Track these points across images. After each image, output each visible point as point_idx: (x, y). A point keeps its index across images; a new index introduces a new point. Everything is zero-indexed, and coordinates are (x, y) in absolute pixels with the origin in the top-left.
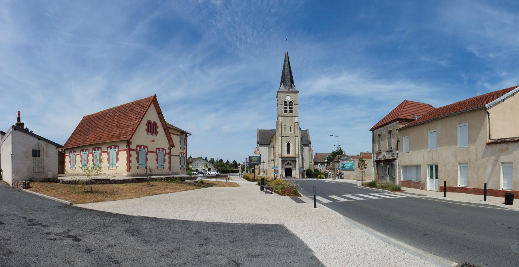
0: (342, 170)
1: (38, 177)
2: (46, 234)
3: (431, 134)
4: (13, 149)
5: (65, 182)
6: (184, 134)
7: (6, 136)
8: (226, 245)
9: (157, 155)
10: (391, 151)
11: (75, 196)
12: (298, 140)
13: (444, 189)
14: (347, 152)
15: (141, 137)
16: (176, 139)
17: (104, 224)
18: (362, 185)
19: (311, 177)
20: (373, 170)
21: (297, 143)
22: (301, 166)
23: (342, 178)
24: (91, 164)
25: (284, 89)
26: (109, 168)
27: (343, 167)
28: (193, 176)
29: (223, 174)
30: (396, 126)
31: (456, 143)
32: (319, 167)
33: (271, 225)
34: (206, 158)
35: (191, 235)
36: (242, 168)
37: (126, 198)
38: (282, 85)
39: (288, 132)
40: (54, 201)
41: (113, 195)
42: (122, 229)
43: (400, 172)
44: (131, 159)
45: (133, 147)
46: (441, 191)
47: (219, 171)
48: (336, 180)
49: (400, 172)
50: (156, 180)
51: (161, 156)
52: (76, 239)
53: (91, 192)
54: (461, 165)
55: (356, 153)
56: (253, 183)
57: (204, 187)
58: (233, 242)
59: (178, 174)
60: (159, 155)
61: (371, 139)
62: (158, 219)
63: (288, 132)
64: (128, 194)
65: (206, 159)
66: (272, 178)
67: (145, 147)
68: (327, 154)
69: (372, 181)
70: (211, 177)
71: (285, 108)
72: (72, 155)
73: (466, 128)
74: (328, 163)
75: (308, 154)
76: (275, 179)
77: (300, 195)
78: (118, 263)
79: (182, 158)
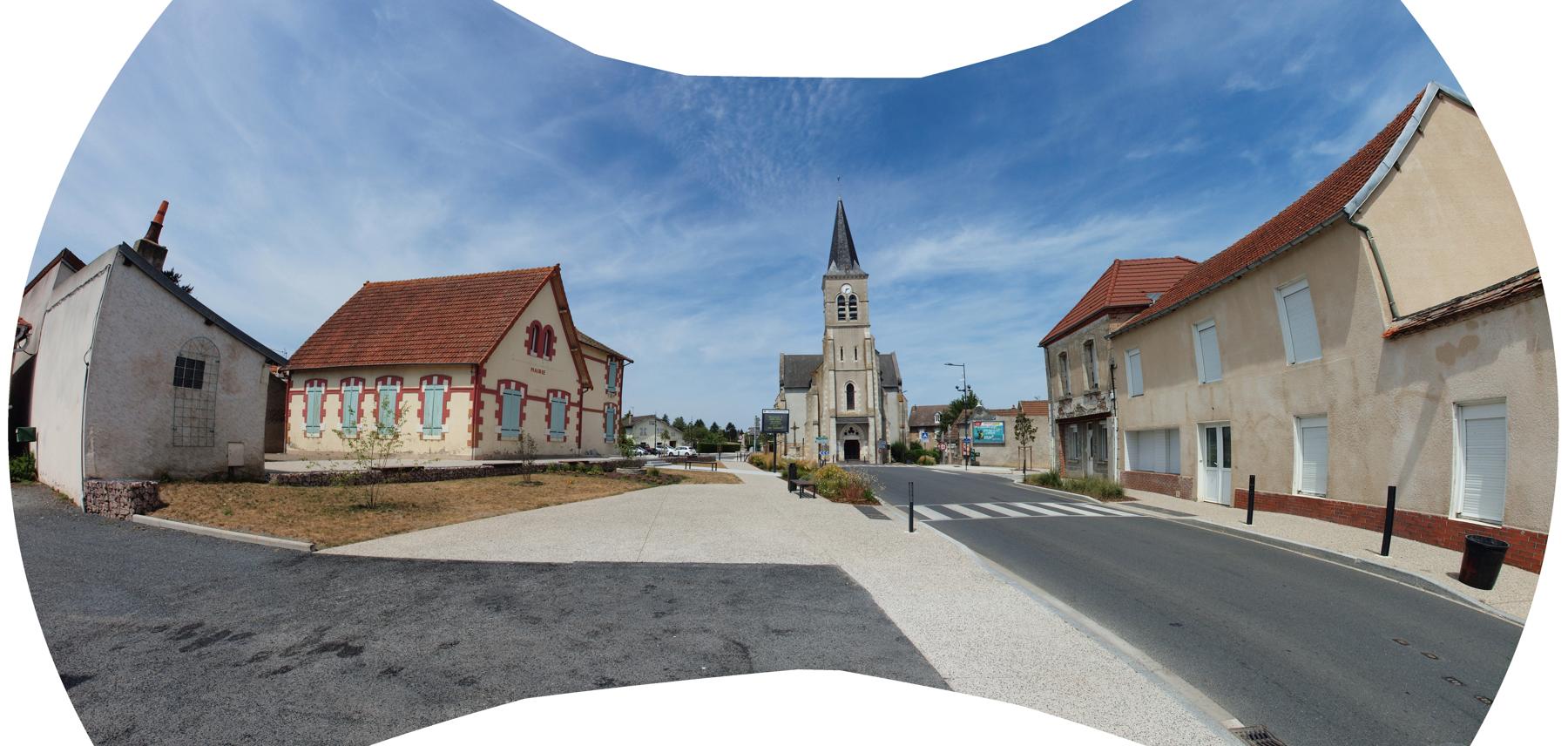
1: (191, 463)
2: (251, 661)
3: (1202, 338)
5: (287, 480)
6: (616, 361)
8: (714, 610)
9: (549, 406)
10: (1097, 394)
12: (872, 379)
13: (1250, 500)
14: (987, 401)
16: (596, 371)
17: (418, 593)
19: (905, 460)
21: (870, 383)
22: (880, 436)
24: (368, 423)
26: (421, 435)
29: (703, 455)
31: (1279, 352)
37: (470, 516)
39: (849, 361)
40: (254, 546)
41: (434, 513)
42: (469, 598)
43: (1121, 449)
44: (482, 413)
45: (489, 382)
46: (1237, 505)
47: (694, 447)
48: (962, 468)
49: (1121, 449)
50: (544, 469)
51: (558, 409)
52: (347, 649)
53: (371, 507)
54: (1305, 424)
58: (733, 603)
59: (598, 455)
61: (1043, 365)
63: (849, 361)
65: (665, 419)
67: (519, 385)
68: (939, 408)
70: (676, 460)
72: (315, 392)
74: (943, 428)
78: (473, 682)
79: (610, 416)
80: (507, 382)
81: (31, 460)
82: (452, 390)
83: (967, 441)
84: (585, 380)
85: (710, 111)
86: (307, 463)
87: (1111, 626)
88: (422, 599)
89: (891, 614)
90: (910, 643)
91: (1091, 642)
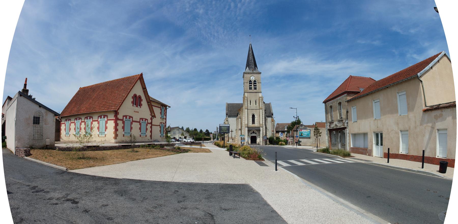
0: (300, 138)
1: (37, 144)
3: (375, 104)
4: (17, 115)
6: (164, 107)
7: (12, 101)
8: (201, 201)
9: (140, 124)
10: (342, 121)
11: (70, 163)
12: (262, 112)
13: (388, 156)
14: (304, 122)
15: (127, 108)
16: (157, 111)
18: (317, 151)
19: (272, 143)
20: (327, 138)
21: (261, 114)
22: (264, 134)
23: (300, 145)
24: (83, 132)
25: (249, 71)
26: (99, 135)
27: (301, 135)
28: (171, 143)
29: (197, 142)
30: (345, 98)
31: (396, 111)
32: (280, 135)
33: (238, 185)
34: (183, 127)
35: (170, 193)
36: (213, 136)
37: (114, 163)
38: (248, 68)
39: (253, 106)
40: (52, 167)
41: (102, 161)
42: (112, 190)
43: (349, 140)
44: (118, 127)
45: (120, 117)
46: (385, 157)
47: (193, 139)
48: (295, 147)
49: (349, 140)
50: (139, 146)
51: (143, 125)
53: (84, 158)
54: (403, 133)
55: (312, 123)
56: (223, 149)
57: (181, 153)
59: (158, 142)
60: (142, 124)
61: (324, 110)
62: (142, 181)
63: (253, 106)
64: (115, 160)
66: (239, 145)
68: (287, 124)
69: (325, 147)
70: (187, 144)
71: (250, 86)
72: (68, 123)
73: (405, 97)
74: (288, 132)
75: (271, 124)
76: (242, 146)
77: (263, 160)
78: (112, 219)
79: (162, 127)
80: (126, 116)
81: (6, 143)
82: (108, 120)
83: (297, 136)
84: (153, 114)
85: (197, 11)
86: (66, 144)
87: (348, 200)
88: (98, 189)
89: (269, 202)
90: (276, 213)
91: (342, 206)
